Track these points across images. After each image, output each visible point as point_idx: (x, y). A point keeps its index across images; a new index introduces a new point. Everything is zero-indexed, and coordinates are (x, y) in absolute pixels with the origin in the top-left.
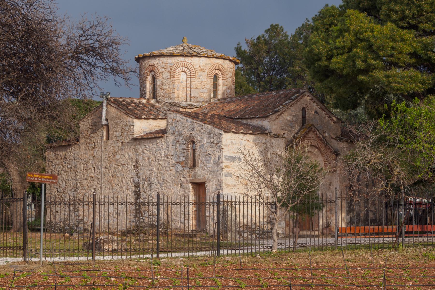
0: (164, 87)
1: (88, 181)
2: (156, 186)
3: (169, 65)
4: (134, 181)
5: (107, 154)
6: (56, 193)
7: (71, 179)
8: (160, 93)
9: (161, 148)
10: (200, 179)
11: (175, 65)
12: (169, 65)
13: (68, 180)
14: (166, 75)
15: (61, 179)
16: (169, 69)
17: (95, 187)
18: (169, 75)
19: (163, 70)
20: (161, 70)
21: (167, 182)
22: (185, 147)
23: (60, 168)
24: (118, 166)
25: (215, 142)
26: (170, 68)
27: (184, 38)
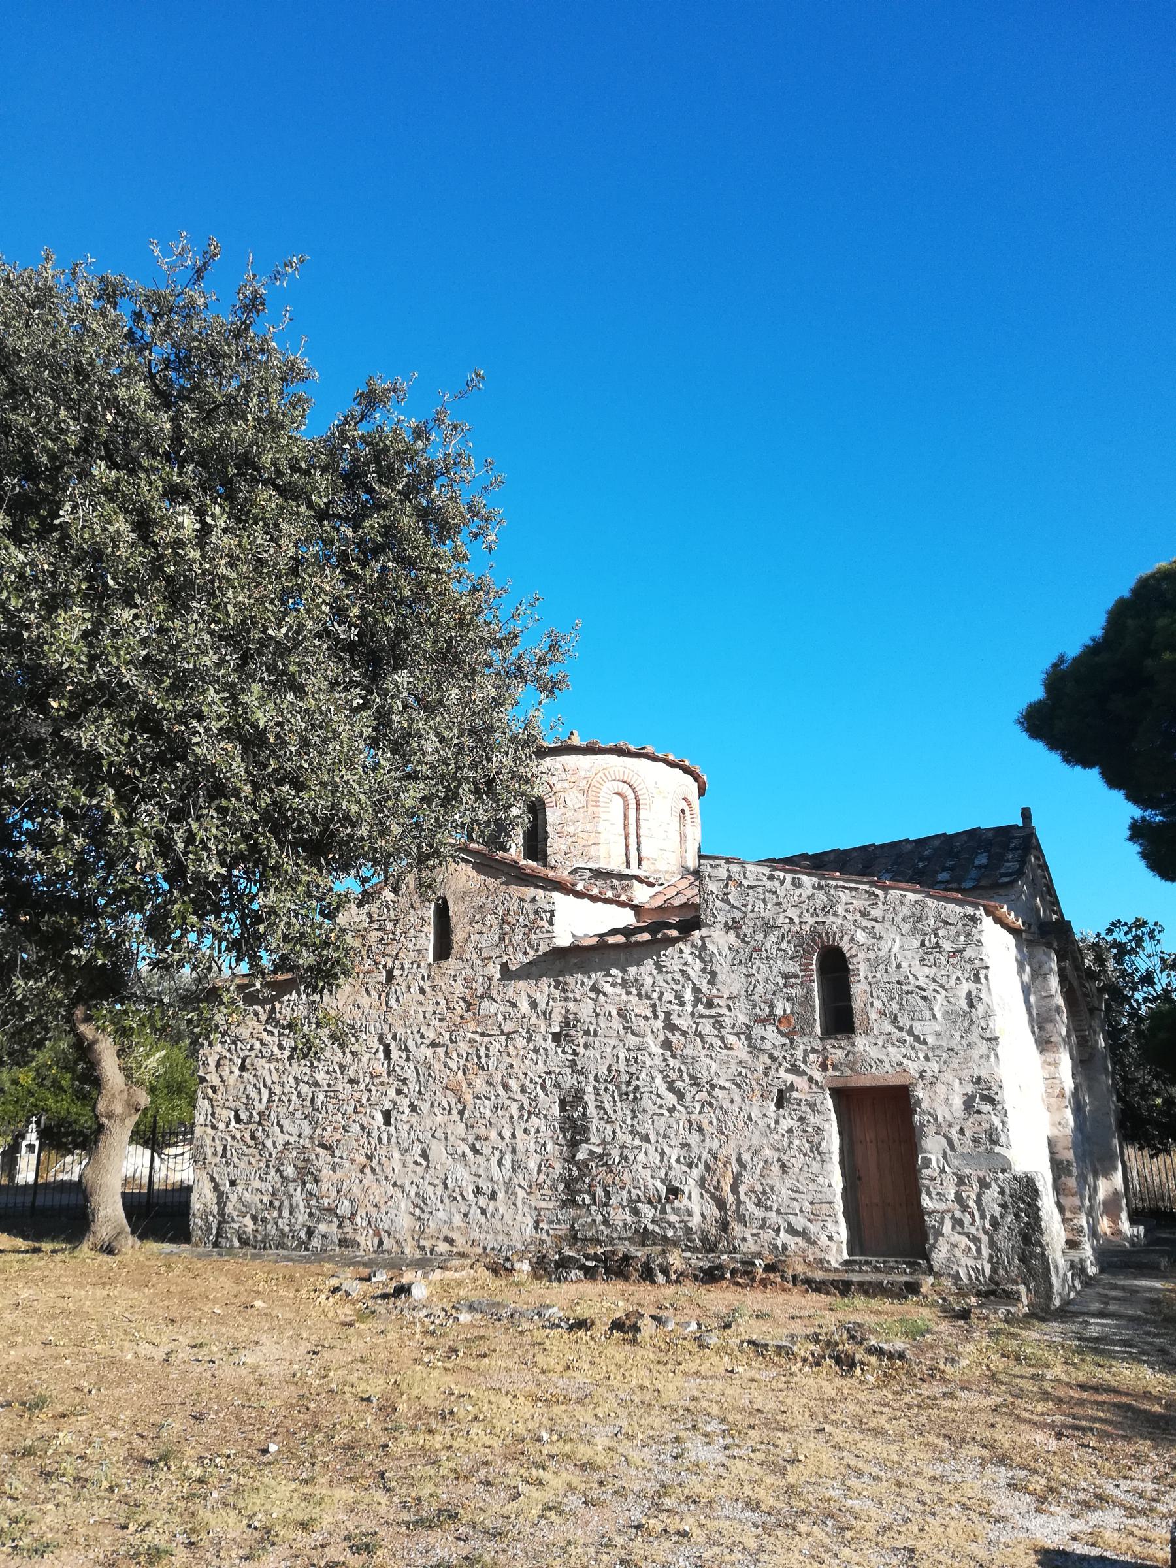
0: (571, 829)
1: (363, 1087)
2: (659, 1101)
3: (582, 773)
4: (558, 1086)
5: (443, 1002)
6: (233, 1123)
7: (291, 1080)
8: (556, 845)
9: (678, 976)
10: (874, 1077)
11: (601, 774)
12: (582, 773)
13: (282, 1084)
14: (574, 798)
15: (253, 1080)
16: (583, 784)
17: (388, 1105)
18: (583, 800)
19: (566, 785)
20: (557, 788)
21: (713, 1087)
22: (793, 967)
23: (252, 1048)
24: (487, 1039)
25: (947, 946)
26: (585, 782)
27: (572, 733)
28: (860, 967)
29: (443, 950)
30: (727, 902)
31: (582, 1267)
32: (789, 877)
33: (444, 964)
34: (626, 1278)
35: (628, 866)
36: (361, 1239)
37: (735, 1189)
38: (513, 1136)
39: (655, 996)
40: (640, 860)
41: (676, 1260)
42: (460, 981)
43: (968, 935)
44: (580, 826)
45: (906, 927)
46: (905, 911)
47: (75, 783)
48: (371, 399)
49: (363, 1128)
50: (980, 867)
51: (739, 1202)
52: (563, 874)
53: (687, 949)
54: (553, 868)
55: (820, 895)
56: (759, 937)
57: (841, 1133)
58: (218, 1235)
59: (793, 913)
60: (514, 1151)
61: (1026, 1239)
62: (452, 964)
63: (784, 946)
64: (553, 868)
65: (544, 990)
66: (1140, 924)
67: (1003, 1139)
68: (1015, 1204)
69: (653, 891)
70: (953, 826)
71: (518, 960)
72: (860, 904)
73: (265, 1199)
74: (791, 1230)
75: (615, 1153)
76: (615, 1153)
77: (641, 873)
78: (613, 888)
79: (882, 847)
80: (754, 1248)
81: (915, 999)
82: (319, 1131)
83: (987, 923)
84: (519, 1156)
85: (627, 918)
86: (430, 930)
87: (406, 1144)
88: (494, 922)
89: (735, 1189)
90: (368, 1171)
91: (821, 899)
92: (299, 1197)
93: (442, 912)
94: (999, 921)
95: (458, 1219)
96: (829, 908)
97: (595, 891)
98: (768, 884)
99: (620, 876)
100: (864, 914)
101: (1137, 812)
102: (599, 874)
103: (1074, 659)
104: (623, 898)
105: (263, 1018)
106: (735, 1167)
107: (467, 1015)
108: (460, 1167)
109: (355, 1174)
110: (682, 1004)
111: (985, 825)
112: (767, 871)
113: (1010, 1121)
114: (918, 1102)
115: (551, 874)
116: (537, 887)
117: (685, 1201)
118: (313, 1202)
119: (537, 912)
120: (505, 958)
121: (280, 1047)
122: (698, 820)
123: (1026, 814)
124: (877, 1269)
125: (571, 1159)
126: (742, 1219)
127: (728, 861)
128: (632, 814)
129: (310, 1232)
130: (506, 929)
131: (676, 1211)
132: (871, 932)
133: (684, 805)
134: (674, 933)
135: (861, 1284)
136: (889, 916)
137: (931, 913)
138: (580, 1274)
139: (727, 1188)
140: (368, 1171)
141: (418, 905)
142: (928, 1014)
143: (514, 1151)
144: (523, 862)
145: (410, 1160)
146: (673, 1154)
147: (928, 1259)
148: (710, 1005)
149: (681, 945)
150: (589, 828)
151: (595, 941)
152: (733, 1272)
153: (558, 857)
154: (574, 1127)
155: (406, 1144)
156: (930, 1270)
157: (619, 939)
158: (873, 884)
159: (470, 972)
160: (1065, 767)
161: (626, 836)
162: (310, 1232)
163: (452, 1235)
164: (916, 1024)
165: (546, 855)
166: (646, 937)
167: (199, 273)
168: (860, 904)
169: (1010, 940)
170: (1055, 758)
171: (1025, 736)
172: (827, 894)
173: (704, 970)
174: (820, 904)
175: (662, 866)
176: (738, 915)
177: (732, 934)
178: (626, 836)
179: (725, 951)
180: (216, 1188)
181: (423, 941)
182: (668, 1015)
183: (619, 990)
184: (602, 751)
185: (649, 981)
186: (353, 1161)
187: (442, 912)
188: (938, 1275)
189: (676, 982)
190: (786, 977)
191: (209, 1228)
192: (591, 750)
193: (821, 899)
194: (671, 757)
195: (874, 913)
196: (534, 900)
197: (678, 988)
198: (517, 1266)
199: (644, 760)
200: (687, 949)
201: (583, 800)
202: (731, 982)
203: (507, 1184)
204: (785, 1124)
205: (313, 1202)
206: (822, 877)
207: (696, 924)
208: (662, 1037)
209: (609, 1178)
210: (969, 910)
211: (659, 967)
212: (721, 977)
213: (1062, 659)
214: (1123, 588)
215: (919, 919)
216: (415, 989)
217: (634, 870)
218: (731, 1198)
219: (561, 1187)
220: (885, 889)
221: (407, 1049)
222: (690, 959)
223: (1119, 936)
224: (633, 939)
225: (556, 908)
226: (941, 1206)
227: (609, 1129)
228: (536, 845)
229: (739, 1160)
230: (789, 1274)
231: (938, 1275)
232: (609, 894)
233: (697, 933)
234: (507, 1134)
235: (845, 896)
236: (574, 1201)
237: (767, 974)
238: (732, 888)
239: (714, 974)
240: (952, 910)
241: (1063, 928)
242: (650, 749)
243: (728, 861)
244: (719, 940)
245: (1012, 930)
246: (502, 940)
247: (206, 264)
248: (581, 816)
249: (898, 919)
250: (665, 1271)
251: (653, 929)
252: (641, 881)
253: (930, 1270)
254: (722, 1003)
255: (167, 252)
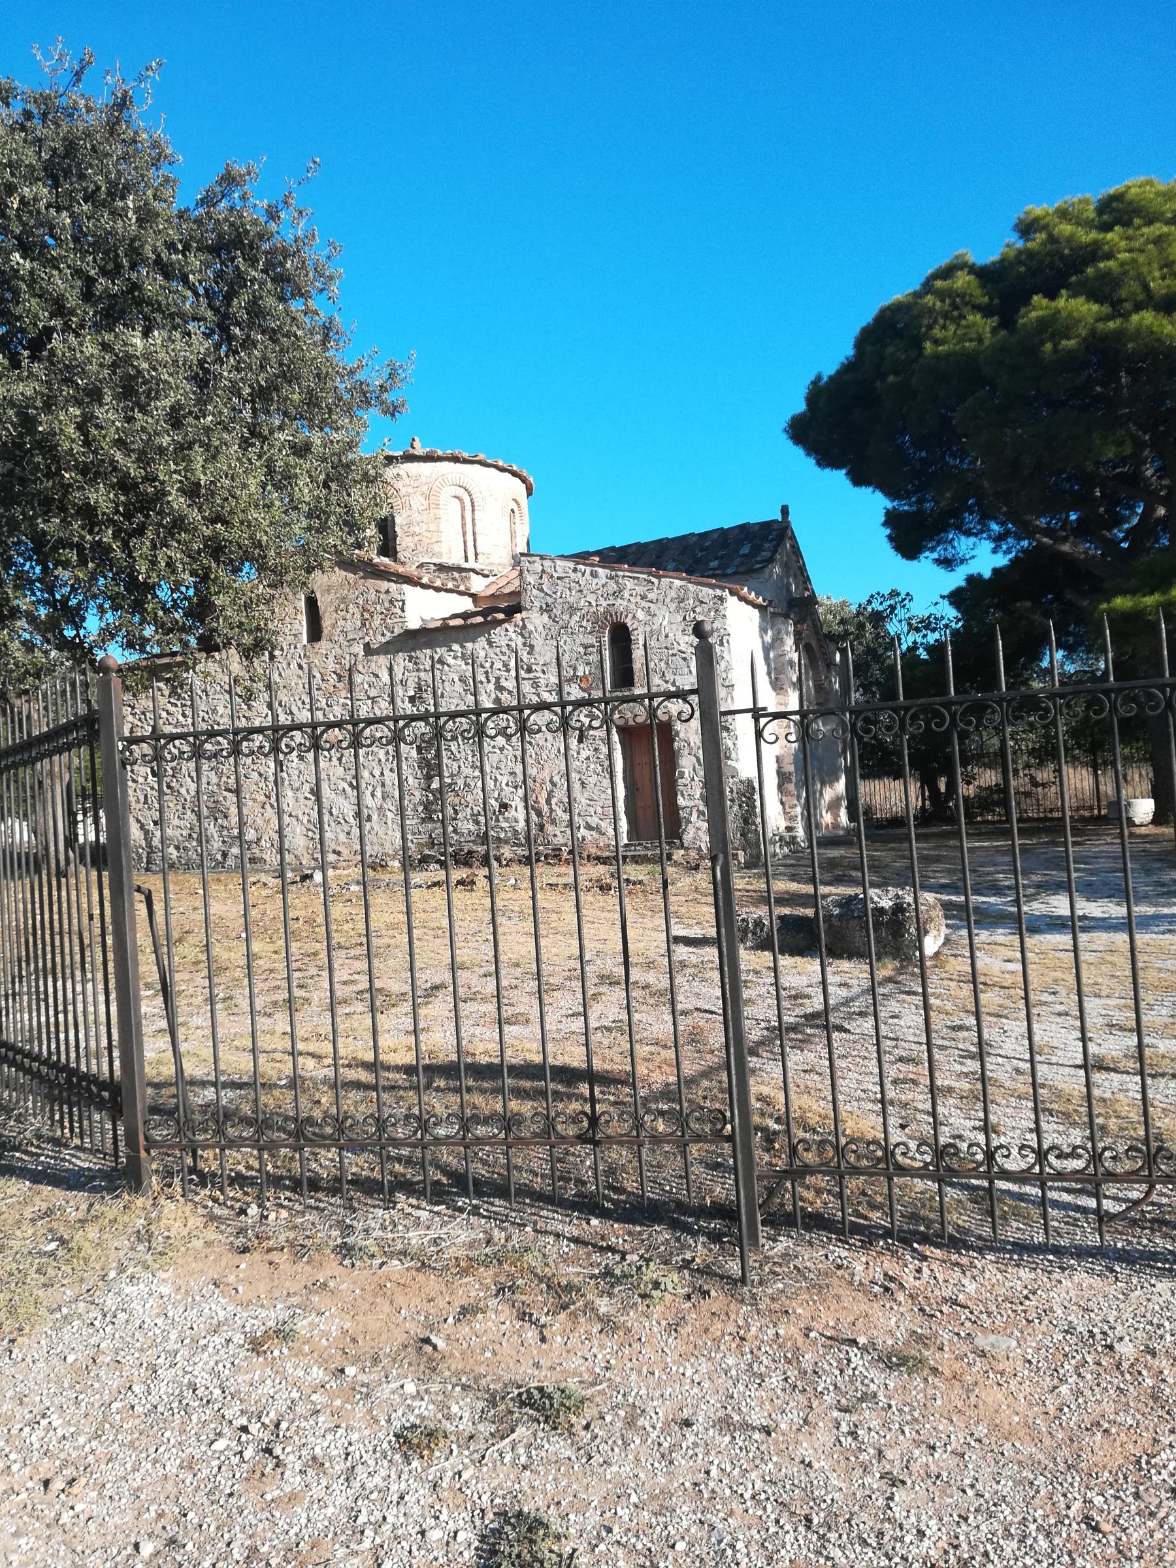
0: (417, 529)
3: (424, 480)
8: (404, 543)
9: (505, 649)
12: (424, 480)
14: (418, 502)
16: (425, 489)
18: (426, 503)
19: (410, 490)
20: (403, 491)
22: (591, 640)
28: (638, 637)
29: (315, 634)
30: (542, 590)
31: (438, 861)
32: (588, 570)
33: (317, 645)
34: (471, 866)
35: (466, 560)
36: (267, 857)
37: (548, 801)
38: (382, 774)
39: (488, 665)
40: (476, 555)
41: (507, 852)
42: (331, 659)
43: (717, 611)
44: (425, 527)
45: (673, 607)
46: (673, 594)
47: (83, 527)
48: (229, 180)
49: (260, 775)
50: (744, 555)
51: (551, 810)
52: (411, 569)
53: (511, 628)
54: (403, 564)
55: (611, 583)
56: (566, 617)
57: (624, 759)
58: (148, 862)
59: (591, 598)
60: (383, 785)
61: (746, 821)
62: (323, 645)
63: (584, 623)
64: (403, 564)
65: (401, 662)
66: (894, 594)
67: (733, 756)
68: (739, 799)
69: (487, 581)
70: (729, 520)
71: (378, 640)
72: (640, 590)
73: (185, 833)
74: (589, 827)
75: (461, 782)
76: (461, 782)
77: (477, 567)
78: (454, 579)
79: (674, 539)
80: (562, 841)
81: (678, 660)
82: (224, 779)
83: (732, 602)
84: (387, 789)
85: (466, 604)
86: (303, 618)
87: (297, 785)
88: (356, 610)
89: (548, 801)
90: (268, 807)
91: (612, 586)
92: (212, 830)
93: (312, 603)
94: (742, 599)
95: (342, 837)
96: (617, 594)
97: (438, 583)
98: (573, 575)
99: (460, 570)
100: (643, 597)
101: (889, 504)
102: (441, 568)
103: (830, 378)
104: (462, 588)
105: (167, 693)
106: (549, 786)
107: (339, 685)
108: (341, 799)
109: (258, 809)
110: (508, 671)
111: (727, 524)
112: (572, 565)
113: (738, 743)
114: (677, 733)
115: (401, 569)
116: (390, 580)
117: (513, 812)
118: (225, 833)
119: (391, 602)
120: (367, 639)
121: (184, 715)
122: (526, 518)
123: (785, 511)
124: (647, 848)
125: (428, 788)
126: (553, 822)
127: (542, 558)
128: (468, 514)
129: (225, 855)
130: (366, 615)
131: (507, 820)
132: (648, 612)
133: (514, 506)
134: (501, 616)
135: (633, 857)
136: (661, 598)
137: (691, 595)
138: (437, 866)
139: (542, 801)
140: (268, 807)
141: (290, 597)
142: (686, 670)
143: (383, 785)
144: (377, 560)
145: (300, 796)
146: (504, 780)
147: (681, 839)
148: (529, 670)
149: (506, 625)
150: (432, 527)
151: (438, 624)
152: (546, 856)
153: (407, 554)
154: (428, 765)
155: (297, 785)
156: (682, 846)
157: (459, 622)
158: (650, 574)
159: (339, 651)
160: (817, 469)
161: (464, 534)
162: (225, 855)
163: (338, 849)
164: (678, 678)
165: (396, 552)
166: (480, 619)
167: (78, 75)
168: (640, 590)
169: (755, 613)
170: (811, 462)
171: (790, 443)
172: (617, 582)
173: (524, 644)
174: (611, 591)
175: (495, 559)
176: (550, 600)
177: (545, 615)
178: (464, 534)
179: (540, 629)
180: (142, 827)
181: (297, 626)
182: (498, 679)
183: (460, 662)
184: (440, 459)
185: (482, 654)
186: (255, 800)
187: (312, 603)
188: (687, 849)
189: (503, 654)
190: (586, 647)
191: (140, 858)
192: (430, 458)
193: (612, 586)
194: (501, 464)
195: (650, 596)
196: (388, 592)
197: (505, 658)
198: (390, 863)
199: (477, 466)
200: (511, 628)
201: (426, 503)
202: (543, 651)
203: (380, 809)
204: (584, 754)
205: (225, 833)
206: (613, 569)
207: (518, 609)
208: (493, 696)
209: (457, 800)
210: (718, 592)
211: (490, 643)
212: (537, 649)
213: (819, 378)
214: (867, 316)
215: (682, 600)
216: (294, 665)
217: (472, 564)
218: (546, 808)
219: (421, 808)
220: (659, 577)
221: (291, 713)
222: (514, 636)
223: (876, 606)
224: (469, 621)
225: (407, 598)
226: (691, 804)
227: (455, 765)
228: (388, 548)
229: (551, 781)
230: (585, 854)
231: (687, 849)
232: (450, 585)
233: (518, 616)
234: (377, 773)
235: (629, 584)
236: (431, 818)
237: (571, 647)
238: (545, 579)
239: (532, 647)
240: (707, 593)
241: (810, 602)
242: (481, 457)
243: (542, 558)
244: (536, 620)
245: (755, 606)
246: (364, 625)
247: (82, 68)
248: (424, 518)
249: (668, 600)
250: (498, 859)
251: (484, 613)
252: (477, 573)
253: (682, 846)
254: (538, 668)
255: (47, 55)
